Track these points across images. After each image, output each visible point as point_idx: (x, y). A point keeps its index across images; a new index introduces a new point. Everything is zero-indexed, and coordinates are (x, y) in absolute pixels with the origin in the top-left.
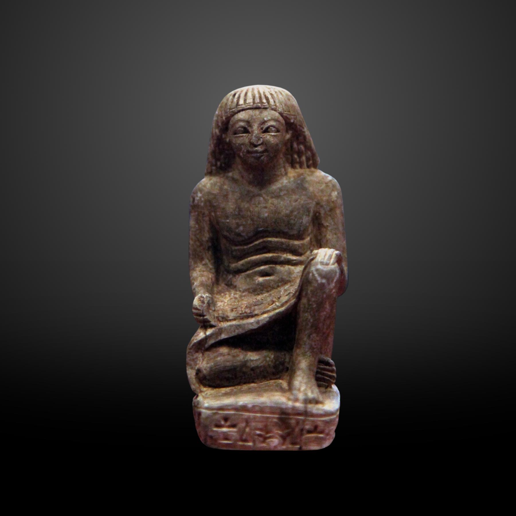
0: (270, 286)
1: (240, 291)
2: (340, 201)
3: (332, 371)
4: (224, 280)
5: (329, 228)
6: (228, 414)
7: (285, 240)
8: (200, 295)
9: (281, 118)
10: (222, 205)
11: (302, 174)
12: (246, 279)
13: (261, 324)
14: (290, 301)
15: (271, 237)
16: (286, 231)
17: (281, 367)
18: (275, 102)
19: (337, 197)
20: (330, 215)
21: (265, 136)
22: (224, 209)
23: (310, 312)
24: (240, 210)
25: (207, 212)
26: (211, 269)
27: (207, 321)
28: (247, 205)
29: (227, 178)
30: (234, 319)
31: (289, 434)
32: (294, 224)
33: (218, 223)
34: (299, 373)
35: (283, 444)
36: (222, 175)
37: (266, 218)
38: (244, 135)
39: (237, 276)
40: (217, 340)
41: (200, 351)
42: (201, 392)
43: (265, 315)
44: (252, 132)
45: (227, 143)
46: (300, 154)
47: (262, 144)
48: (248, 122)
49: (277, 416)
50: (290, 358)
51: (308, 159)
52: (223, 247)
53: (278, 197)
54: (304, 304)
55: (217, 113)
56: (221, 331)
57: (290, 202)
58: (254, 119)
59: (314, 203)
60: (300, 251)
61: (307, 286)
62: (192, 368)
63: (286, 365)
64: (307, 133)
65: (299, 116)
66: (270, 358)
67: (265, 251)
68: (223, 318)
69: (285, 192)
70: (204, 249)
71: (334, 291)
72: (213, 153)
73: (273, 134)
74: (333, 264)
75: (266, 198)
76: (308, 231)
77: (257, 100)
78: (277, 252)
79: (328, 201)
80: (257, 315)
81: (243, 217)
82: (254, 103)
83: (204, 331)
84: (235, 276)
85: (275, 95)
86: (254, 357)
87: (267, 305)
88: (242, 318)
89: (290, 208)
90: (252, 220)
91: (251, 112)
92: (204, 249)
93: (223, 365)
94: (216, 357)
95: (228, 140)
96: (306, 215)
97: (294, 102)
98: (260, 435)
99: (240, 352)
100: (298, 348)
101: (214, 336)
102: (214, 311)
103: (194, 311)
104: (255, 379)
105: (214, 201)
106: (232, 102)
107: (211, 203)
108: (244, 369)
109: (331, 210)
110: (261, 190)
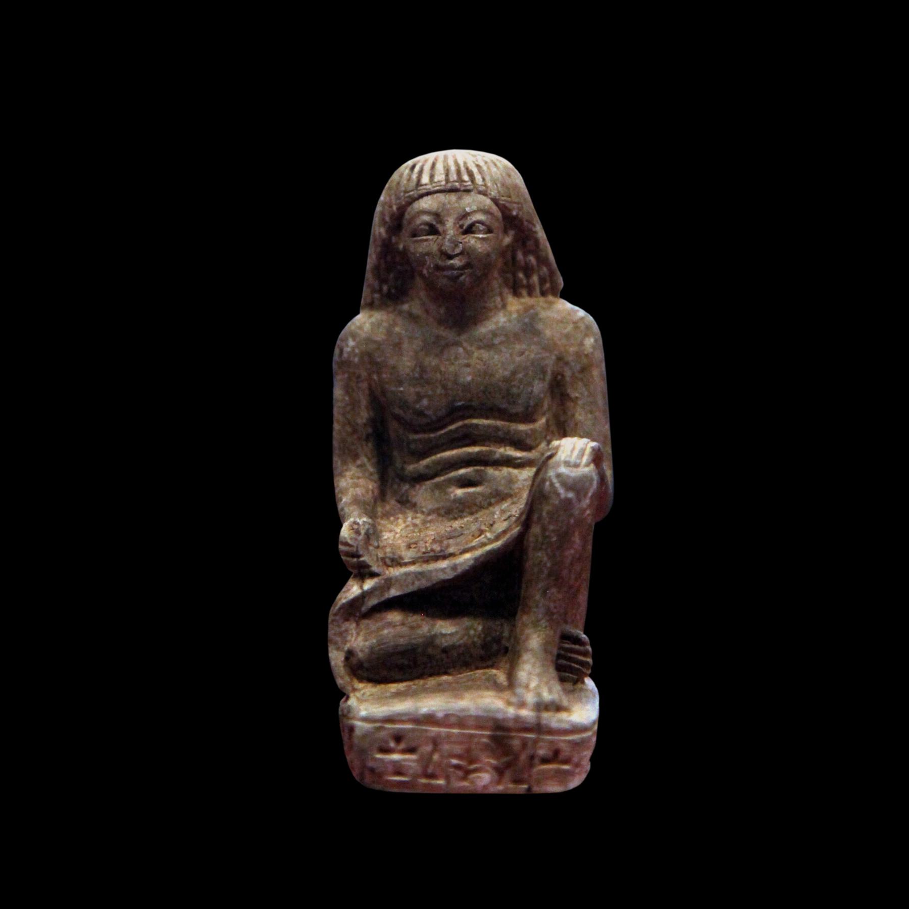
0: (475, 505)
1: (423, 512)
3: (585, 654)
4: (395, 493)
5: (580, 402)
6: (401, 729)
7: (502, 423)
8: (352, 519)
9: (495, 208)
10: (392, 362)
11: (532, 307)
12: (433, 491)
13: (459, 570)
14: (512, 530)
15: (477, 418)
16: (504, 406)
17: (495, 647)
18: (484, 179)
19: (594, 347)
20: (582, 379)
21: (466, 240)
22: (394, 367)
23: (546, 549)
24: (423, 370)
25: (364, 374)
26: (371, 474)
27: (365, 566)
28: (434, 362)
29: (400, 313)
30: (413, 563)
31: (508, 765)
32: (519, 395)
33: (384, 392)
34: (526, 657)
35: (499, 782)
36: (390, 309)
37: (469, 383)
38: (430, 237)
39: (418, 486)
40: (383, 599)
41: (352, 619)
42: (354, 690)
43: (468, 556)
44: (445, 232)
45: (399, 253)
46: (528, 270)
47: (461, 253)
48: (437, 215)
49: (488, 733)
50: (511, 631)
51: (542, 281)
52: (392, 435)
53: (490, 346)
54: (536, 536)
56: (389, 583)
57: (511, 355)
58: (448, 210)
59: (554, 357)
60: (529, 441)
61: (541, 504)
62: (338, 649)
63: (504, 643)
66: (475, 630)
67: (467, 442)
68: (393, 560)
69: (503, 338)
70: (359, 439)
71: (588, 512)
73: (481, 236)
74: (587, 465)
75: (469, 348)
76: (542, 406)
77: (453, 177)
78: (487, 443)
79: (578, 355)
80: (452, 555)
81: (428, 382)
82: (447, 181)
83: (360, 583)
84: (413, 486)
85: (485, 168)
86: (447, 630)
87: (470, 537)
88: (427, 561)
89: (512, 367)
90: (444, 387)
91: (441, 197)
92: (359, 439)
93: (392, 643)
94: (380, 629)
95: (401, 247)
96: (540, 379)
97: (517, 179)
98: (457, 767)
99: (423, 620)
100: (524, 612)
101: (377, 593)
102: (378, 547)
104: (449, 668)
105: (376, 355)
106: (409, 180)
108: (430, 651)
109: (583, 370)
110: (459, 335)
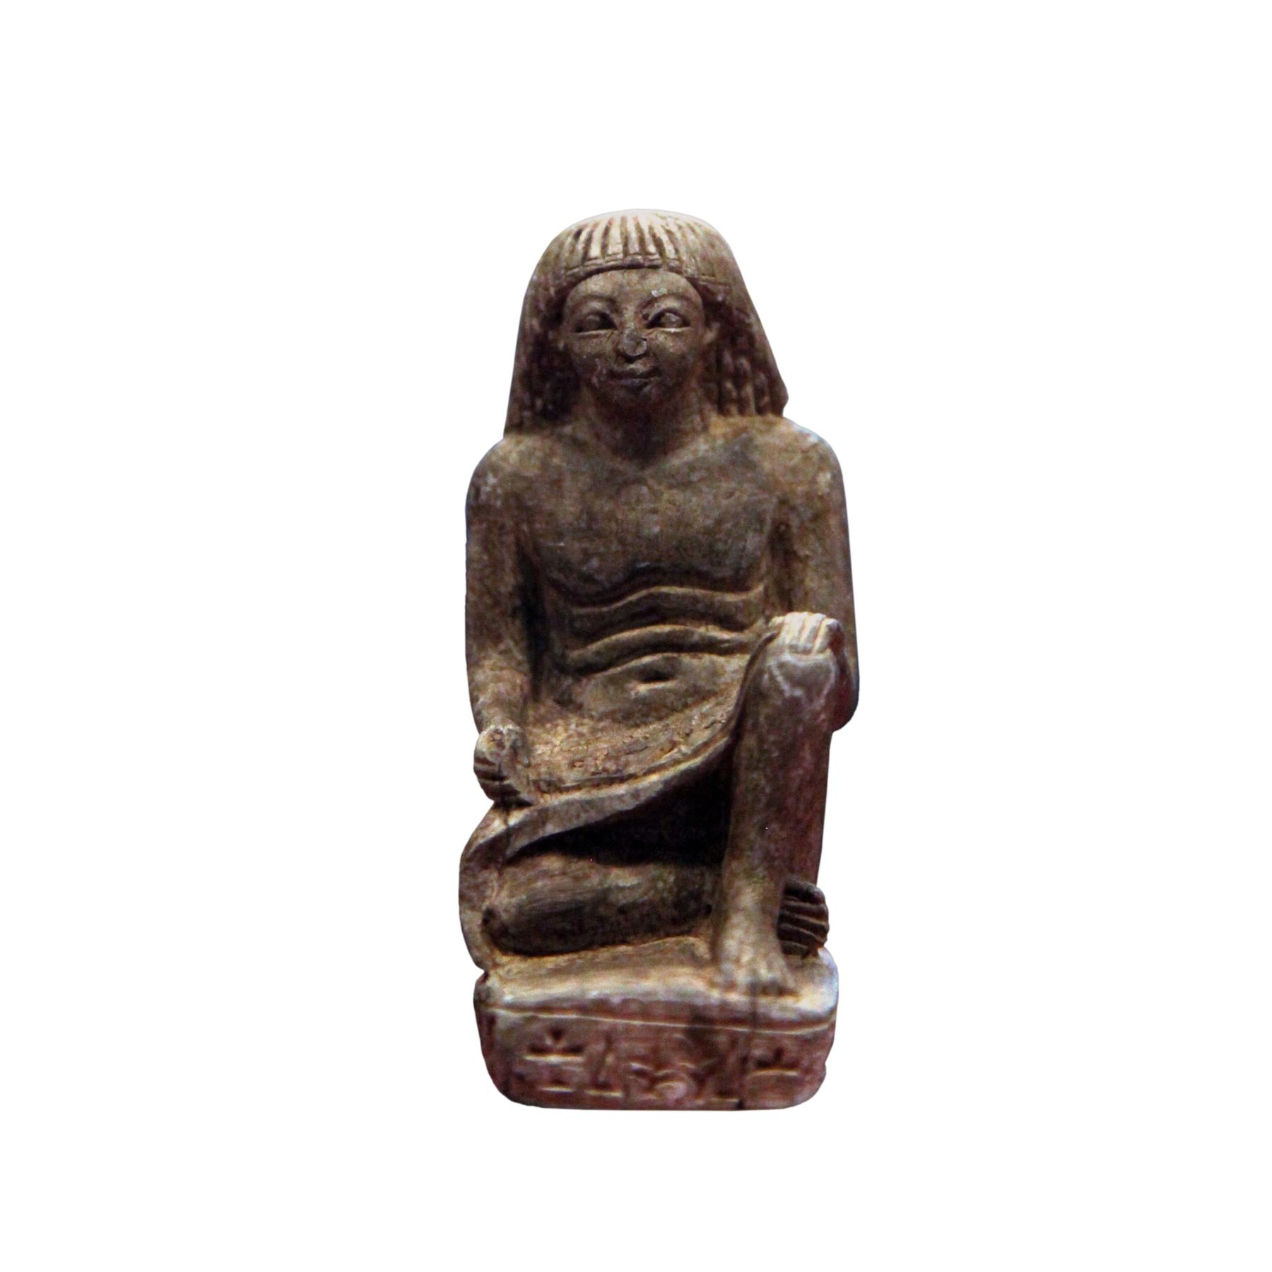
0: (665, 706)
1: (592, 717)
4: (553, 689)
5: (812, 563)
6: (562, 1020)
7: (703, 592)
8: (492, 727)
9: (692, 292)
10: (548, 506)
11: (745, 429)
12: (605, 687)
13: (643, 798)
14: (716, 741)
15: (667, 585)
16: (705, 568)
17: (693, 905)
18: (677, 251)
20: (814, 531)
21: (653, 336)
22: (551, 514)
23: (764, 769)
24: (592, 518)
25: (509, 523)
26: (520, 664)
28: (608, 506)
29: (560, 438)
30: (578, 788)
31: (711, 1071)
32: (726, 553)
33: (537, 549)
34: (736, 919)
35: (698, 1094)
36: (546, 432)
37: (656, 537)
38: (602, 332)
39: (585, 681)
40: (535, 838)
41: (492, 866)
43: (654, 778)
44: (622, 324)
45: (559, 354)
46: (739, 378)
47: (646, 354)
48: (611, 301)
49: (683, 1026)
50: (715, 883)
51: (759, 393)
52: (549, 609)
53: (685, 485)
54: (750, 750)
56: (544, 816)
57: (715, 497)
58: (627, 294)
59: (775, 500)
60: (740, 618)
61: (757, 705)
63: (706, 899)
66: (665, 881)
67: (654, 618)
68: (549, 784)
69: (703, 473)
70: (503, 614)
71: (823, 716)
73: (673, 330)
74: (822, 651)
75: (656, 487)
76: (759, 568)
77: (634, 247)
78: (682, 620)
79: (809, 497)
80: (633, 777)
81: (599, 535)
82: (626, 253)
83: (503, 815)
84: (578, 681)
85: (678, 235)
86: (626, 881)
87: (658, 751)
88: (597, 785)
89: (716, 514)
90: (622, 542)
91: (618, 276)
92: (503, 614)
93: (549, 900)
94: (531, 880)
95: (561, 345)
96: (755, 530)
98: (640, 1073)
99: (591, 868)
100: (734, 857)
101: (528, 829)
102: (529, 766)
104: (628, 934)
105: (527, 496)
106: (572, 251)
108: (602, 910)
109: (816, 517)
110: (643, 468)
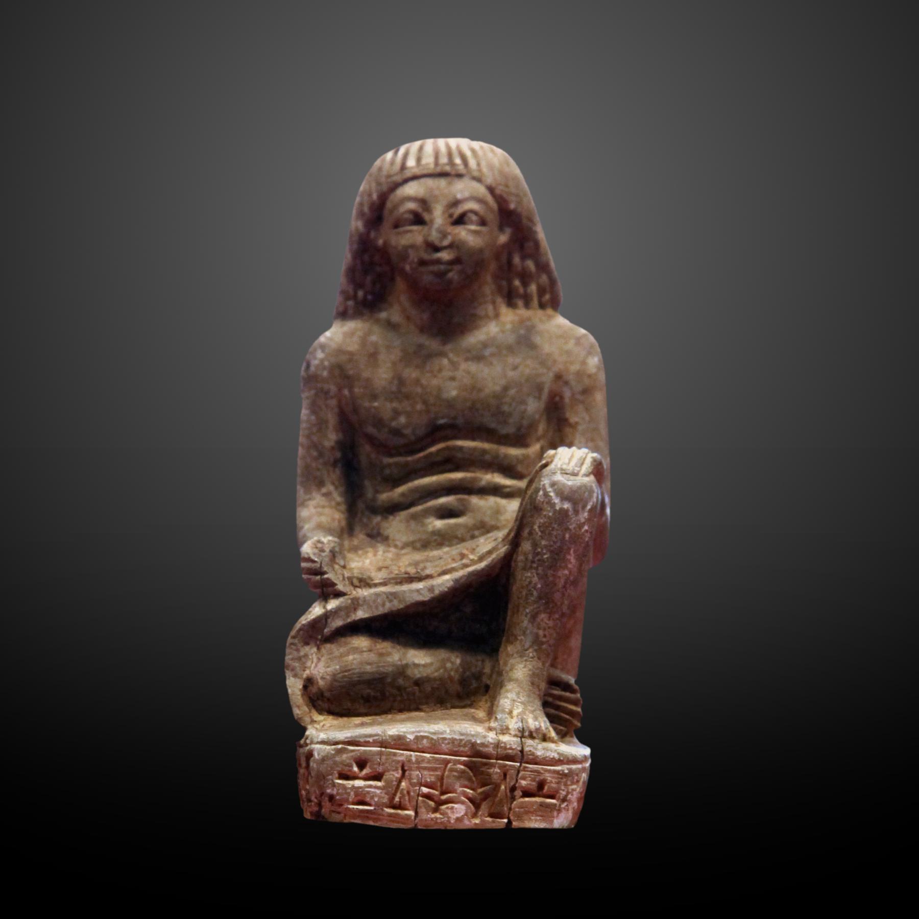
0: (456, 537)
1: (396, 546)
2: (602, 377)
3: (575, 703)
5: (580, 428)
6: (365, 751)
8: (315, 538)
9: (489, 198)
10: (366, 374)
11: (529, 319)
12: (408, 521)
13: (437, 592)
16: (493, 425)
18: (479, 165)
19: (598, 368)
22: (368, 380)
23: (537, 569)
24: (401, 382)
29: (378, 321)
30: (384, 584)
31: (486, 796)
32: (510, 415)
33: (356, 410)
34: (509, 686)
35: (475, 815)
37: (454, 399)
38: (415, 228)
39: (391, 517)
40: (349, 620)
41: (312, 644)
43: (447, 577)
44: (432, 221)
45: (378, 250)
46: (525, 278)
47: (451, 246)
48: (424, 203)
50: (493, 668)
51: (541, 291)
52: (364, 460)
53: (479, 358)
54: (525, 554)
55: (362, 188)
56: (356, 604)
58: (436, 197)
59: (551, 375)
60: (520, 468)
61: (532, 516)
62: (295, 676)
63: (485, 680)
64: (541, 235)
65: (527, 200)
66: (452, 663)
67: (449, 466)
68: (361, 580)
70: (325, 464)
71: (586, 528)
72: (351, 273)
74: (587, 475)
75: (455, 359)
76: (536, 431)
77: (444, 160)
78: (471, 469)
79: (579, 374)
81: (407, 397)
83: (323, 603)
84: (386, 518)
86: (421, 660)
87: (450, 560)
89: (503, 382)
90: (425, 402)
91: (430, 182)
93: (357, 671)
94: (341, 656)
95: (380, 242)
96: (535, 397)
97: (515, 170)
98: (428, 796)
100: (509, 642)
101: (343, 613)
102: (344, 567)
103: (304, 565)
104: (422, 704)
107: (342, 372)
108: (401, 681)
